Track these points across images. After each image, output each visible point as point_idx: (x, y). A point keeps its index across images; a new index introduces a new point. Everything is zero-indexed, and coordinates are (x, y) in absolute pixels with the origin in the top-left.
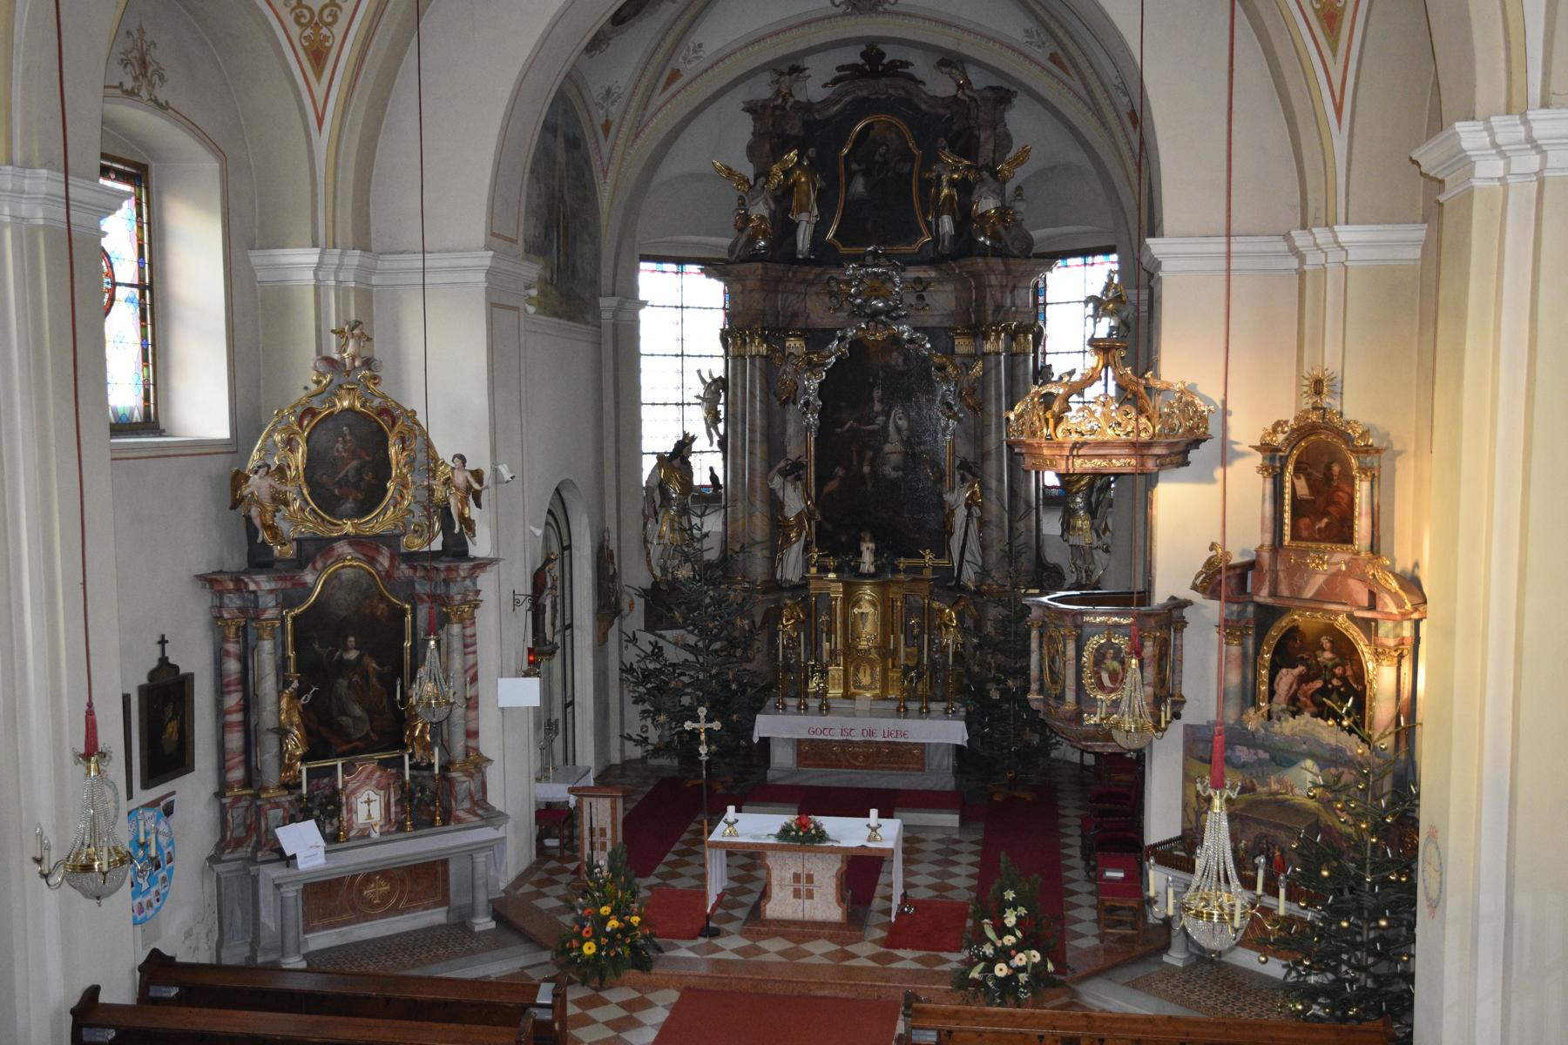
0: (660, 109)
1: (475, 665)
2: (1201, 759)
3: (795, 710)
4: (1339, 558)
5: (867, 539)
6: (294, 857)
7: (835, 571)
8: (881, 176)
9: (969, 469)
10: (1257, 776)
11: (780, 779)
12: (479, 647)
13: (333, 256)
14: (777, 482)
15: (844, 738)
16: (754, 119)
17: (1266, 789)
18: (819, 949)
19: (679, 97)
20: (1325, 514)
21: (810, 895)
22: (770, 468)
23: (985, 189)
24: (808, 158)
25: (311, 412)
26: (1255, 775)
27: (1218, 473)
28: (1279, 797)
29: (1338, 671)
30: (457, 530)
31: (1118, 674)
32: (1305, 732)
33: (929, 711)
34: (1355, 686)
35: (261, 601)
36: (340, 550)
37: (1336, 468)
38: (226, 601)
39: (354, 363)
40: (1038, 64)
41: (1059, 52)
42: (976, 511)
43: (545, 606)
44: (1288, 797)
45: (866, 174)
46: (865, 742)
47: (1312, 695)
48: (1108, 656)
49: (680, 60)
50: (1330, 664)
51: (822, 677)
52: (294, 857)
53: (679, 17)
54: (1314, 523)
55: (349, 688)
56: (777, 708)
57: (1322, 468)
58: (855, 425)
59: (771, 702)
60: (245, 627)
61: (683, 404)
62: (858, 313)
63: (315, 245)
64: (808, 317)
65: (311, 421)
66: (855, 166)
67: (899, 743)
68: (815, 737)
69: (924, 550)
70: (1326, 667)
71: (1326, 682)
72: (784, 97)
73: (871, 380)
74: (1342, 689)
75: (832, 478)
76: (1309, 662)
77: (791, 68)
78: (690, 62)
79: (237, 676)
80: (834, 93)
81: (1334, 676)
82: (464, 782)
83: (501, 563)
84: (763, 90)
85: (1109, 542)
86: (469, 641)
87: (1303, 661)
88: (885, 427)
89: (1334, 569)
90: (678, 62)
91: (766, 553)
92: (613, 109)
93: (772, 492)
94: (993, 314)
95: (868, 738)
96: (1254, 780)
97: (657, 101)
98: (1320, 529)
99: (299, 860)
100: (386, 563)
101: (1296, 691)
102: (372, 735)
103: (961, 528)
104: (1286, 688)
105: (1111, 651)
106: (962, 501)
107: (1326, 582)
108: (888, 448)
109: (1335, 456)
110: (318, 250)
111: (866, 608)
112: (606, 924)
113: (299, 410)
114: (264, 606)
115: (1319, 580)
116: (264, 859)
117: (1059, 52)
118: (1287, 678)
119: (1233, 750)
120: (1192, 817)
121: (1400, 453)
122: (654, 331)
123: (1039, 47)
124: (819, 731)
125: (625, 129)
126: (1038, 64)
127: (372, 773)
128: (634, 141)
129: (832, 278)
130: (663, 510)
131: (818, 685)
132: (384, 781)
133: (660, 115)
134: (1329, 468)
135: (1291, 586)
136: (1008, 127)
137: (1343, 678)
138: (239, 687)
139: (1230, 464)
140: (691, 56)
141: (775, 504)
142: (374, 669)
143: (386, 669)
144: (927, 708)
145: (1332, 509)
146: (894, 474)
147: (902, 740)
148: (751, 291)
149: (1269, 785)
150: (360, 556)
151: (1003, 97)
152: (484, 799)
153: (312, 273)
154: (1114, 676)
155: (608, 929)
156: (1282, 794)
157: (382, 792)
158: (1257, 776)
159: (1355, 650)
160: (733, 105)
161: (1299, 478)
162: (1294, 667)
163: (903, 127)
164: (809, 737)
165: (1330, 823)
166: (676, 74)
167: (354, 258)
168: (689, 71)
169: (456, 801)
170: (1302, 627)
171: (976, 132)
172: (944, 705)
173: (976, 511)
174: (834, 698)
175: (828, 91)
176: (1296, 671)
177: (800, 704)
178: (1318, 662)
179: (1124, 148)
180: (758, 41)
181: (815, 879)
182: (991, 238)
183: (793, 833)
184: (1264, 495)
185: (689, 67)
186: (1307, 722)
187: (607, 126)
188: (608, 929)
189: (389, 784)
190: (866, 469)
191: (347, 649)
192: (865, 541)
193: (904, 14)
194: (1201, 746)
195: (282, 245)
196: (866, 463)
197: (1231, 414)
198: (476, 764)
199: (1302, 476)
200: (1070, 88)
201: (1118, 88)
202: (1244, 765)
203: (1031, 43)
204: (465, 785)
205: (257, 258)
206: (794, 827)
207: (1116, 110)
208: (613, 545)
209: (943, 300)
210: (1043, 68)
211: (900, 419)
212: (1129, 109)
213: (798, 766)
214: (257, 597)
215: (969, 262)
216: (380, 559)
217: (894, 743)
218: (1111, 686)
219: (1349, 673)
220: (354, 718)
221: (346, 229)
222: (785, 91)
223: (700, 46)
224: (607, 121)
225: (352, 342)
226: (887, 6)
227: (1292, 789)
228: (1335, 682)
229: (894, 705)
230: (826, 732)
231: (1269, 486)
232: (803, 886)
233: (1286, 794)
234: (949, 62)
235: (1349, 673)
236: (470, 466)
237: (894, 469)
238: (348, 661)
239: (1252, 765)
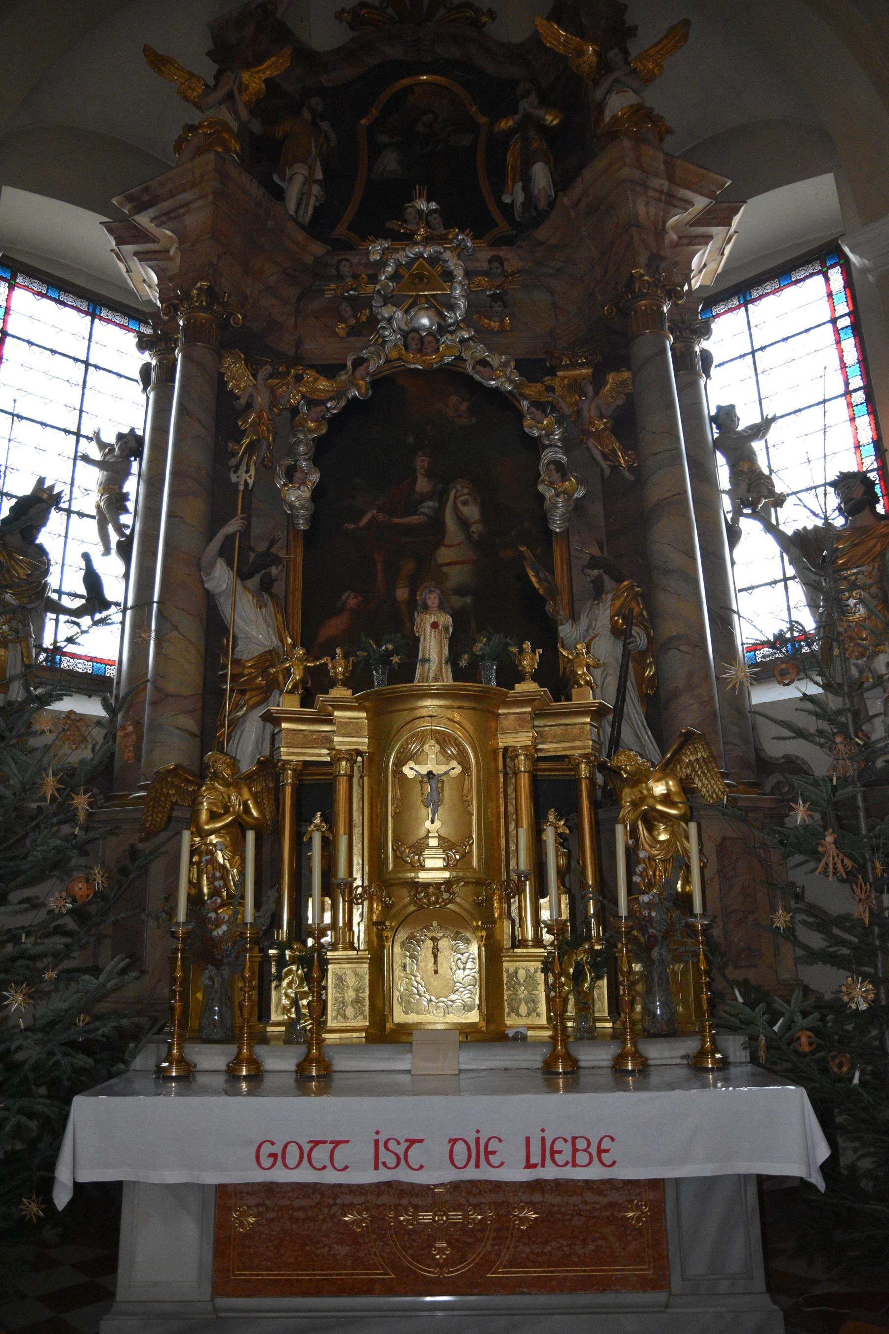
3: (219, 1081)
7: (346, 684)
15: (384, 1175)
18: (266, 944)
33: (644, 1068)
42: (640, 638)
46: (455, 1186)
51: (307, 978)
56: (162, 1075)
58: (381, 517)
59: (143, 1061)
66: (384, 139)
67: (588, 1184)
68: (280, 1175)
73: (411, 440)
88: (436, 524)
91: (189, 723)
95: (471, 1174)
108: (444, 555)
124: (293, 1153)
131: (295, 1002)
144: (637, 1055)
147: (594, 1173)
164: (257, 1176)
172: (690, 1046)
173: (640, 638)
174: (345, 1047)
177: (238, 1061)
192: (426, 608)
211: (465, 503)
213: (218, 1290)
217: (560, 1186)
229: (534, 1059)
230: (321, 1154)
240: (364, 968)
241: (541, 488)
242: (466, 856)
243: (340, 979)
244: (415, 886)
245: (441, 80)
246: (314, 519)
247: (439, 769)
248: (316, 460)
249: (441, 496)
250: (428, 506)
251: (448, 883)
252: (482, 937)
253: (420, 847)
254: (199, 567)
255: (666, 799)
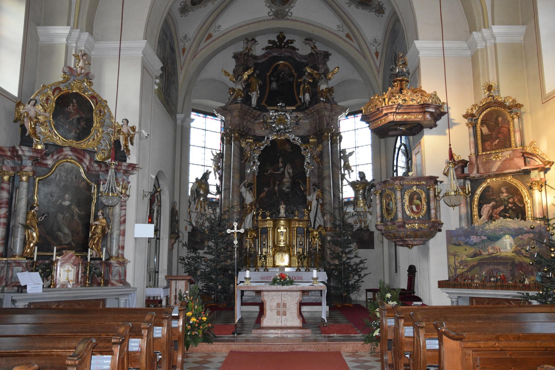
0: (203, 48)
1: (125, 215)
2: (455, 245)
4: (507, 153)
5: (282, 203)
6: (25, 287)
7: (269, 216)
8: (282, 82)
9: (317, 186)
10: (482, 248)
11: (247, 300)
12: (127, 208)
13: (76, 32)
14: (243, 189)
16: (236, 61)
17: (487, 253)
19: (211, 45)
20: (497, 138)
21: (285, 314)
22: (240, 184)
23: (322, 81)
24: (256, 74)
25: (58, 88)
26: (481, 247)
27: (447, 131)
28: (494, 255)
29: (511, 200)
30: (122, 149)
31: (419, 206)
32: (502, 226)
34: (520, 205)
35: (24, 163)
36: (66, 153)
37: (500, 119)
38: (6, 163)
39: (81, 71)
40: (341, 38)
41: (350, 33)
42: (321, 201)
43: (154, 210)
44: (498, 254)
45: (277, 81)
47: (500, 213)
48: (415, 198)
49: (212, 30)
50: (506, 198)
52: (25, 287)
53: (214, 12)
54: (492, 143)
55: (63, 219)
57: (494, 120)
58: (272, 172)
60: (14, 177)
61: (204, 166)
62: (272, 130)
63: (68, 25)
64: (255, 131)
65: (59, 93)
66: (273, 79)
69: (304, 209)
70: (505, 200)
71: (505, 207)
72: (249, 50)
73: (278, 155)
74: (514, 208)
75: (263, 192)
76: (497, 199)
77: (251, 40)
78: (216, 32)
79: (6, 200)
80: (266, 53)
81: (509, 203)
82: (117, 266)
83: (140, 171)
84: (240, 47)
85: (372, 211)
86: (123, 204)
87: (493, 200)
88: (283, 173)
89: (504, 158)
90: (211, 31)
92: (187, 44)
93: (241, 193)
94: (326, 126)
96: (481, 250)
97: (202, 45)
98: (495, 145)
99: (28, 289)
100: (87, 163)
101: (492, 213)
102: (73, 243)
103: (314, 208)
104: (487, 213)
105: (416, 196)
106: (315, 197)
107: (501, 164)
108: (285, 180)
109: (499, 114)
110: (69, 27)
111: (282, 229)
112: (190, 320)
113: (53, 88)
114: (25, 165)
115: (498, 164)
116: (8, 291)
117: (350, 33)
118: (486, 209)
119: (469, 238)
120: (453, 271)
121: (524, 113)
122: (195, 137)
123: (342, 32)
124: (265, 278)
125: (190, 53)
126: (341, 38)
127: (71, 256)
128: (193, 59)
129: (265, 115)
130: (198, 199)
132: (77, 262)
133: (203, 50)
134: (497, 119)
135: (485, 169)
136: (328, 66)
137: (514, 203)
138: (7, 206)
139: (452, 128)
140: (216, 29)
141: (242, 199)
142: (76, 211)
143: (82, 213)
145: (500, 136)
146: (287, 190)
148: (235, 117)
149: (488, 250)
150: (75, 158)
151: (327, 55)
152: (125, 280)
153: (65, 39)
154: (418, 206)
155: (191, 322)
156: (495, 253)
157: (75, 267)
158: (482, 248)
159: (517, 190)
160: (228, 54)
161: (483, 127)
162: (489, 203)
163: (290, 66)
165: (521, 260)
166: (210, 36)
167: (86, 36)
168: (215, 35)
169: (112, 275)
170: (491, 185)
171: (318, 66)
173: (321, 201)
175: (264, 52)
176: (491, 205)
178: (501, 199)
179: (373, 67)
180: (241, 27)
181: (287, 305)
182: (325, 98)
183: (278, 281)
184: (469, 134)
185: (215, 34)
186: (502, 221)
187: (184, 50)
188: (191, 322)
189: (79, 264)
190: (276, 188)
191: (64, 200)
192: (281, 204)
193: (294, 20)
194: (454, 239)
195: (53, 23)
196: (276, 186)
197: (450, 108)
198: (123, 263)
199: (485, 126)
200: (353, 47)
201: (371, 44)
202: (475, 244)
203: (339, 30)
204: (116, 268)
205: (41, 30)
206: (279, 278)
207: (370, 52)
208: (177, 209)
209: (306, 125)
210: (344, 40)
212: (375, 51)
214: (22, 160)
215: (318, 106)
216: (85, 160)
218: (417, 211)
219: (516, 200)
220: (64, 234)
221: (84, 22)
222: (249, 48)
223: (220, 26)
224: (184, 48)
225: (82, 61)
226: (288, 17)
227: (500, 250)
228: (510, 205)
230: (268, 278)
231: (471, 130)
232: (281, 310)
233: (497, 253)
234: (309, 39)
235: (516, 200)
236: (130, 125)
237: (288, 188)
238: (64, 205)
239: (479, 243)
240: (272, 258)
241: (305, 167)
242: (287, 243)
243: (268, 260)
244: (279, 247)
245: (287, 63)
246: (259, 173)
247: (283, 231)
248: (259, 160)
249: (285, 167)
250: (282, 169)
251: (284, 246)
252: (66, 252)
253: (280, 241)
254: (239, 187)
255: (316, 235)
